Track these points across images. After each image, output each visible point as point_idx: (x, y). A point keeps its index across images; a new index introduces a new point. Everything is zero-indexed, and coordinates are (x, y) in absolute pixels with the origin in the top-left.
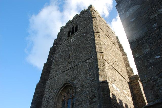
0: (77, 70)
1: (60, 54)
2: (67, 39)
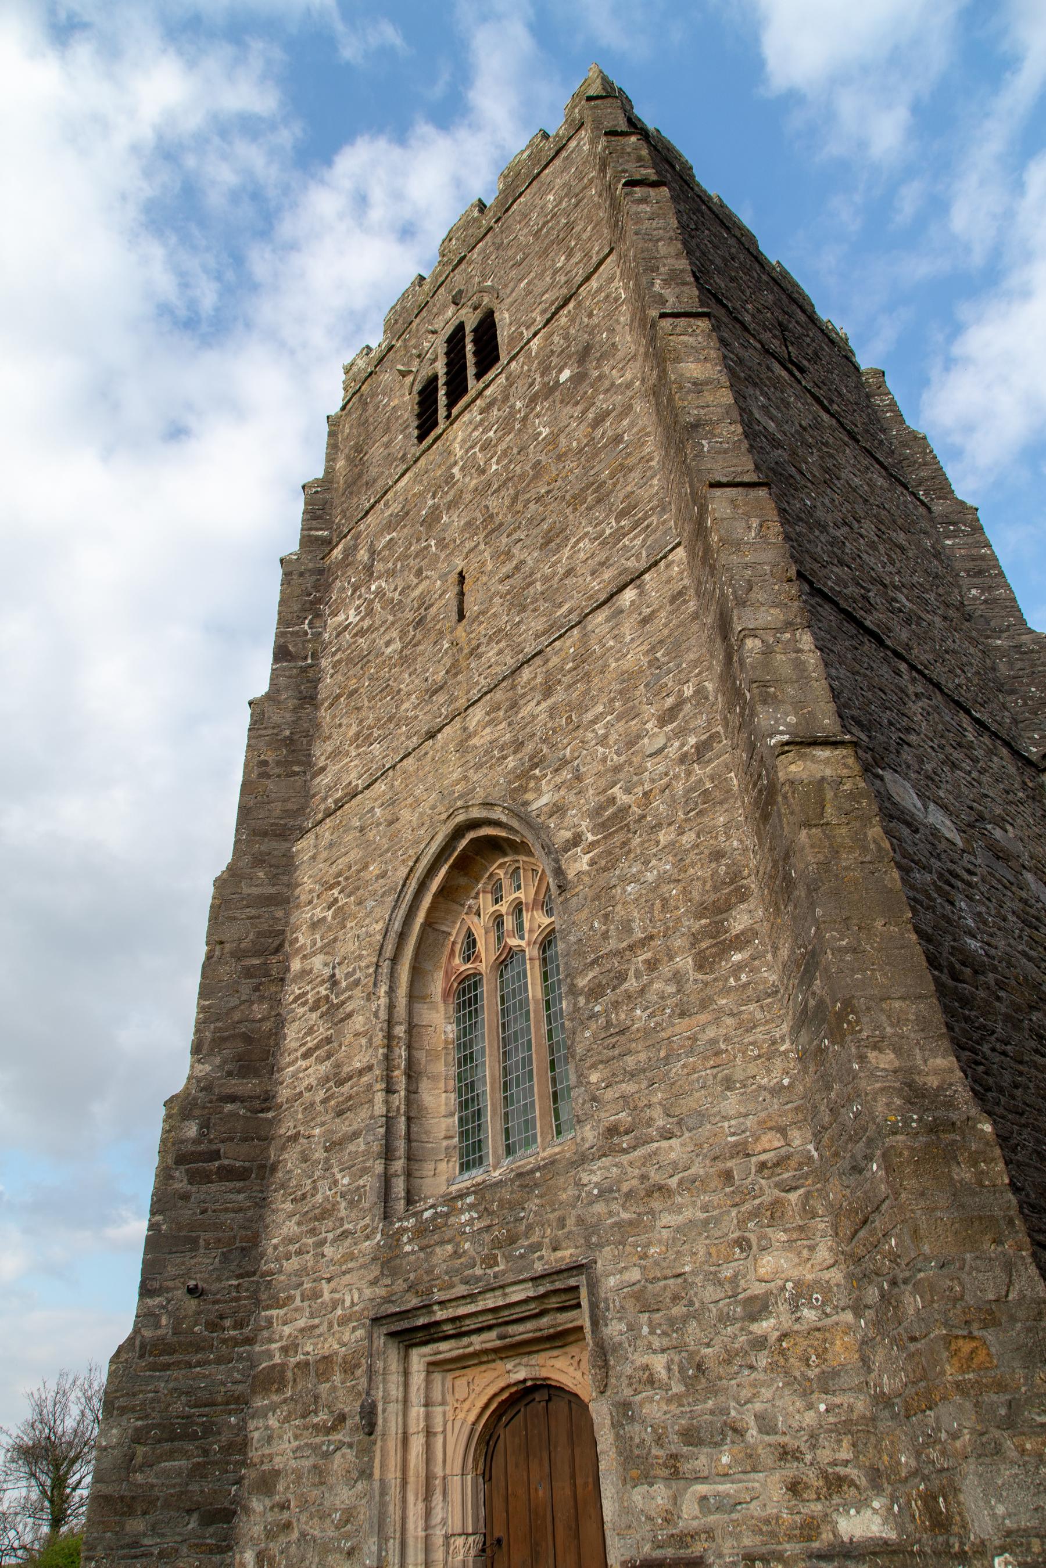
0: (548, 692)
1: (380, 593)
2: (416, 450)
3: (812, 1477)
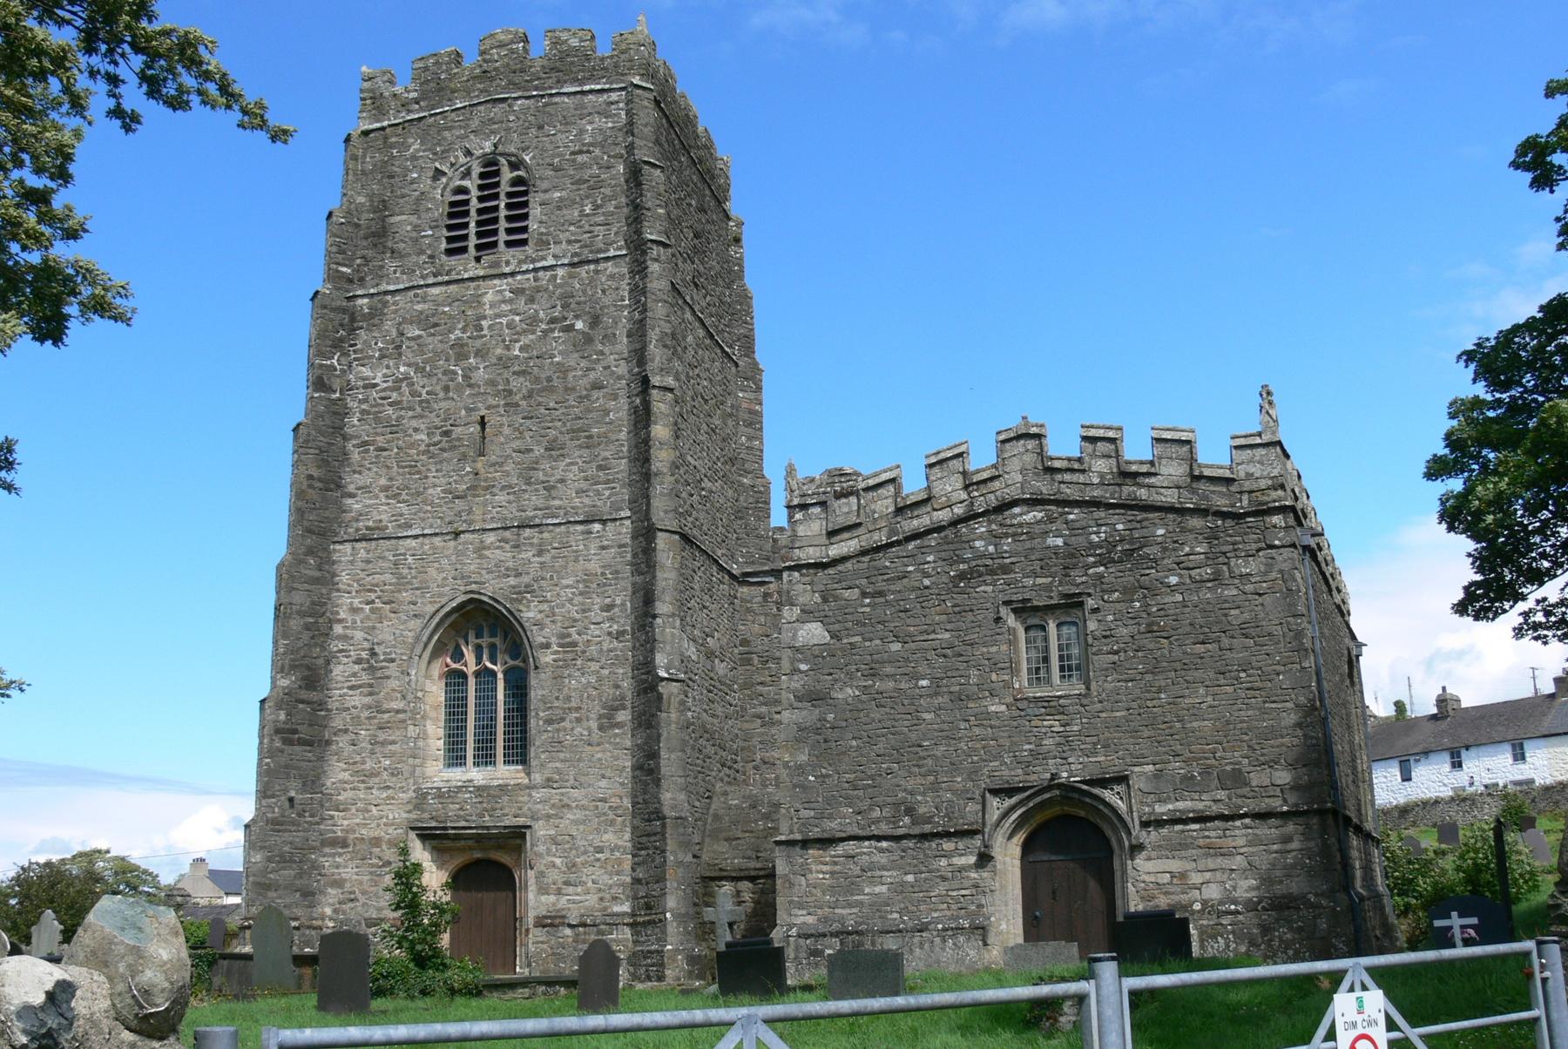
3: (608, 896)
